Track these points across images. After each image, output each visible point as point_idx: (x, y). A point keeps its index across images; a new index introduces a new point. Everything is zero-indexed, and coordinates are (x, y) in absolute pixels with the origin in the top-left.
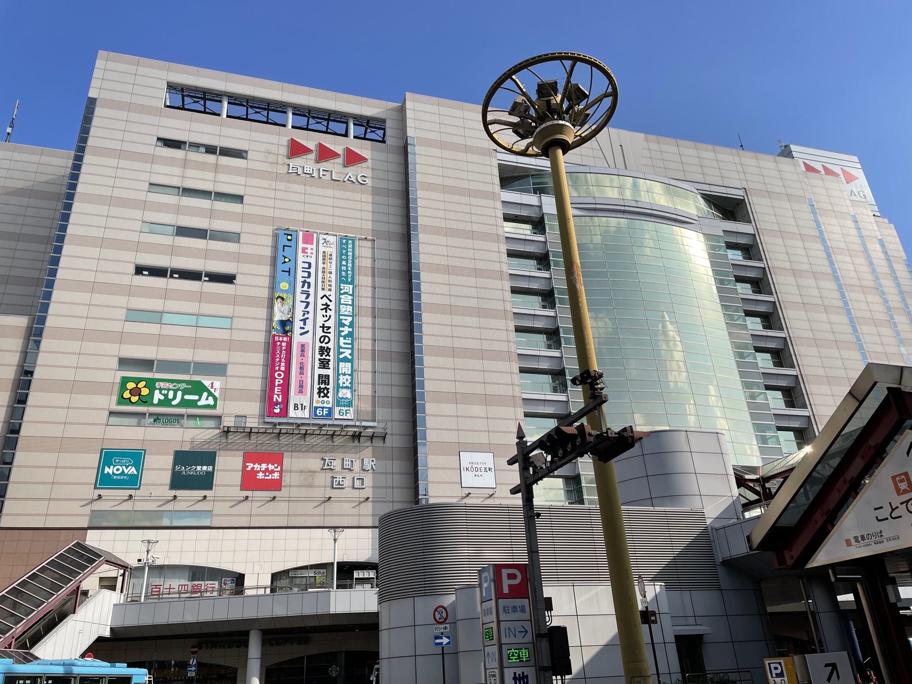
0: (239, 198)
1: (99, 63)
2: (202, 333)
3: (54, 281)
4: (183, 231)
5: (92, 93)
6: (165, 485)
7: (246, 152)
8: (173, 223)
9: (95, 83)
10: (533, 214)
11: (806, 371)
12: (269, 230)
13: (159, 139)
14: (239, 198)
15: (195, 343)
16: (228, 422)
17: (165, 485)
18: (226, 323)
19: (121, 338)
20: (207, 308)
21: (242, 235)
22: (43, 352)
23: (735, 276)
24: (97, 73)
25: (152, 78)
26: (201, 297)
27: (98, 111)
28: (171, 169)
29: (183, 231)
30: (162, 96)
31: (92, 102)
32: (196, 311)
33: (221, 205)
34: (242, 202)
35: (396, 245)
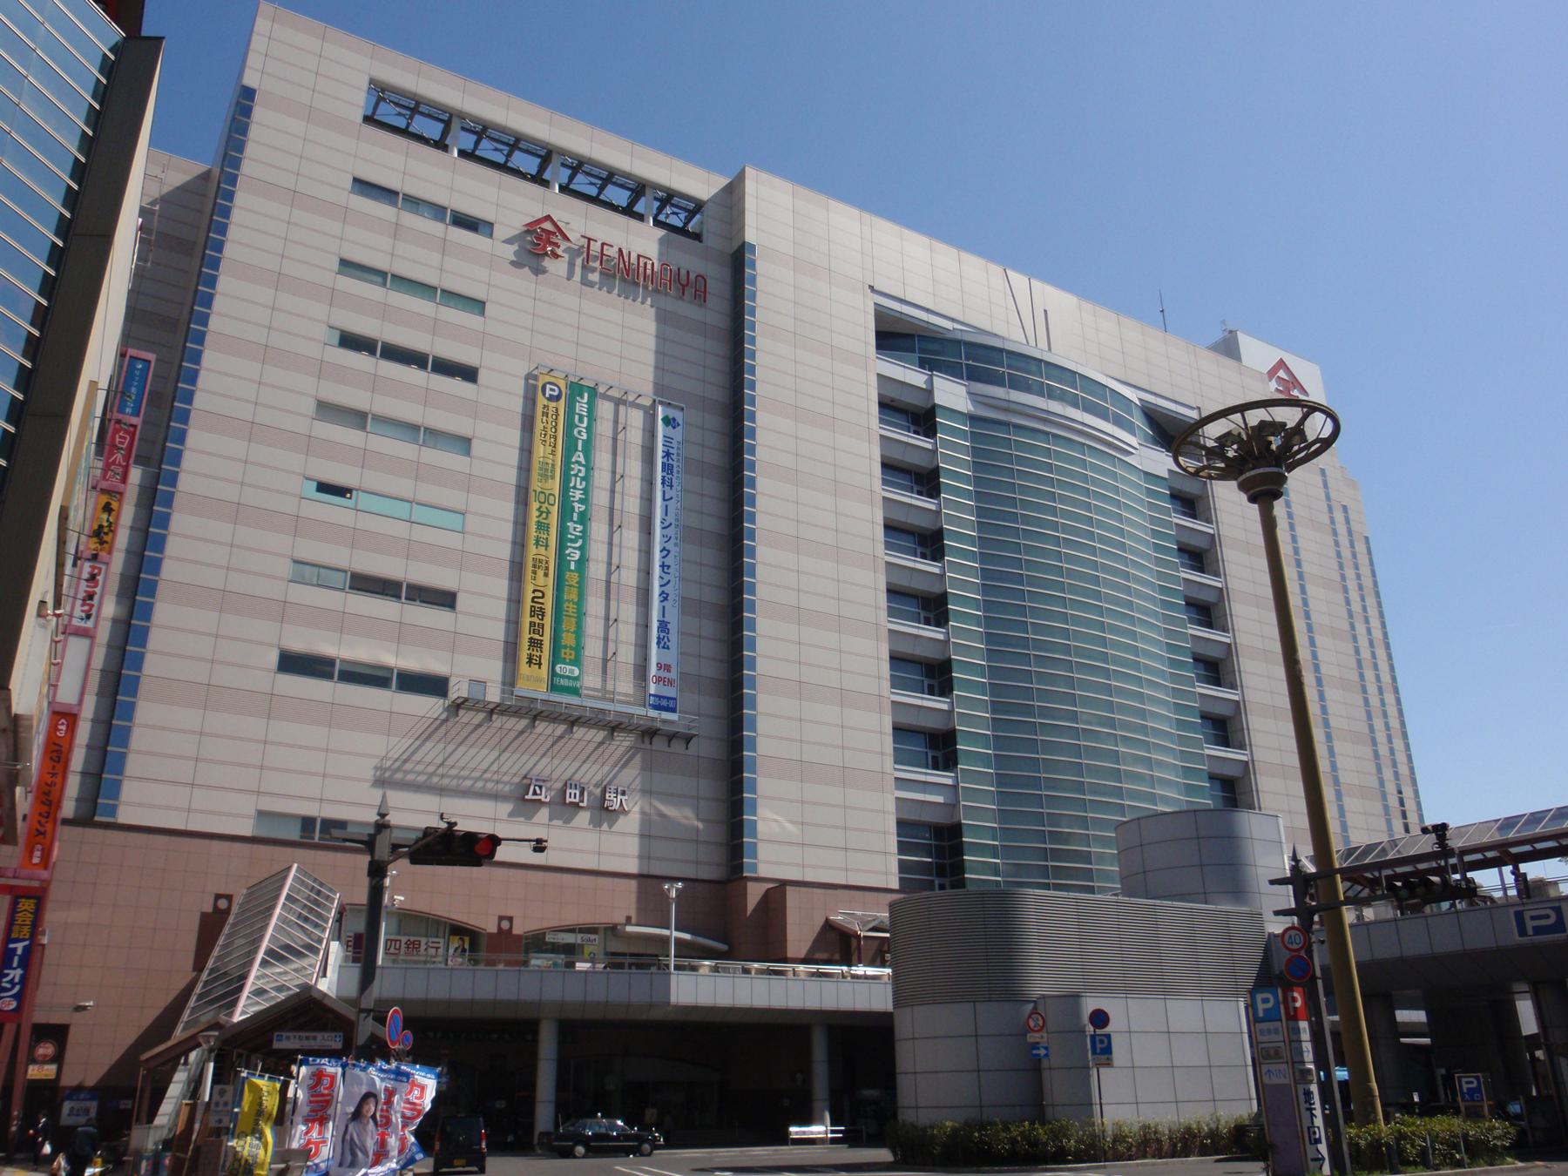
0: (478, 306)
1: (262, 24)
2: (419, 533)
3: (138, 678)
4: (364, 584)
5: (250, 80)
6: (365, 780)
7: (491, 225)
8: (343, 563)
9: (254, 60)
10: (925, 523)
11: (1250, 696)
12: (523, 368)
13: (356, 180)
14: (478, 306)
15: (410, 549)
16: (458, 690)
17: (365, 780)
18: (454, 521)
19: (283, 611)
20: (427, 492)
21: (474, 442)
22: (128, 804)
23: (1178, 543)
24: (258, 43)
25: (348, 67)
26: (410, 549)
27: (259, 113)
28: (375, 236)
29: (364, 584)
30: (359, 102)
31: (249, 93)
32: (409, 495)
33: (451, 315)
34: (482, 313)
35: (713, 487)
